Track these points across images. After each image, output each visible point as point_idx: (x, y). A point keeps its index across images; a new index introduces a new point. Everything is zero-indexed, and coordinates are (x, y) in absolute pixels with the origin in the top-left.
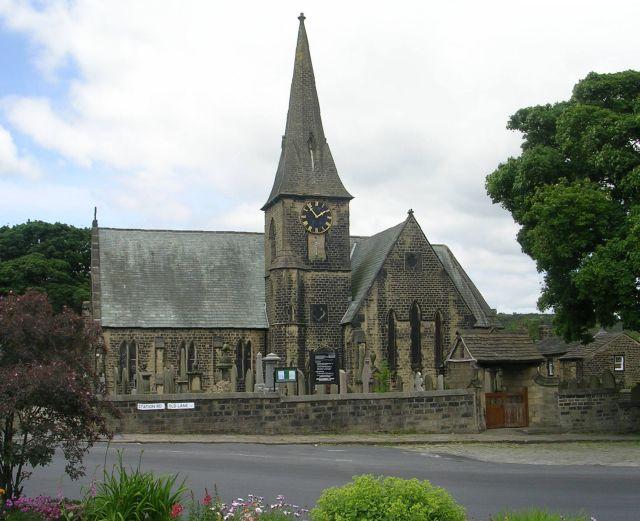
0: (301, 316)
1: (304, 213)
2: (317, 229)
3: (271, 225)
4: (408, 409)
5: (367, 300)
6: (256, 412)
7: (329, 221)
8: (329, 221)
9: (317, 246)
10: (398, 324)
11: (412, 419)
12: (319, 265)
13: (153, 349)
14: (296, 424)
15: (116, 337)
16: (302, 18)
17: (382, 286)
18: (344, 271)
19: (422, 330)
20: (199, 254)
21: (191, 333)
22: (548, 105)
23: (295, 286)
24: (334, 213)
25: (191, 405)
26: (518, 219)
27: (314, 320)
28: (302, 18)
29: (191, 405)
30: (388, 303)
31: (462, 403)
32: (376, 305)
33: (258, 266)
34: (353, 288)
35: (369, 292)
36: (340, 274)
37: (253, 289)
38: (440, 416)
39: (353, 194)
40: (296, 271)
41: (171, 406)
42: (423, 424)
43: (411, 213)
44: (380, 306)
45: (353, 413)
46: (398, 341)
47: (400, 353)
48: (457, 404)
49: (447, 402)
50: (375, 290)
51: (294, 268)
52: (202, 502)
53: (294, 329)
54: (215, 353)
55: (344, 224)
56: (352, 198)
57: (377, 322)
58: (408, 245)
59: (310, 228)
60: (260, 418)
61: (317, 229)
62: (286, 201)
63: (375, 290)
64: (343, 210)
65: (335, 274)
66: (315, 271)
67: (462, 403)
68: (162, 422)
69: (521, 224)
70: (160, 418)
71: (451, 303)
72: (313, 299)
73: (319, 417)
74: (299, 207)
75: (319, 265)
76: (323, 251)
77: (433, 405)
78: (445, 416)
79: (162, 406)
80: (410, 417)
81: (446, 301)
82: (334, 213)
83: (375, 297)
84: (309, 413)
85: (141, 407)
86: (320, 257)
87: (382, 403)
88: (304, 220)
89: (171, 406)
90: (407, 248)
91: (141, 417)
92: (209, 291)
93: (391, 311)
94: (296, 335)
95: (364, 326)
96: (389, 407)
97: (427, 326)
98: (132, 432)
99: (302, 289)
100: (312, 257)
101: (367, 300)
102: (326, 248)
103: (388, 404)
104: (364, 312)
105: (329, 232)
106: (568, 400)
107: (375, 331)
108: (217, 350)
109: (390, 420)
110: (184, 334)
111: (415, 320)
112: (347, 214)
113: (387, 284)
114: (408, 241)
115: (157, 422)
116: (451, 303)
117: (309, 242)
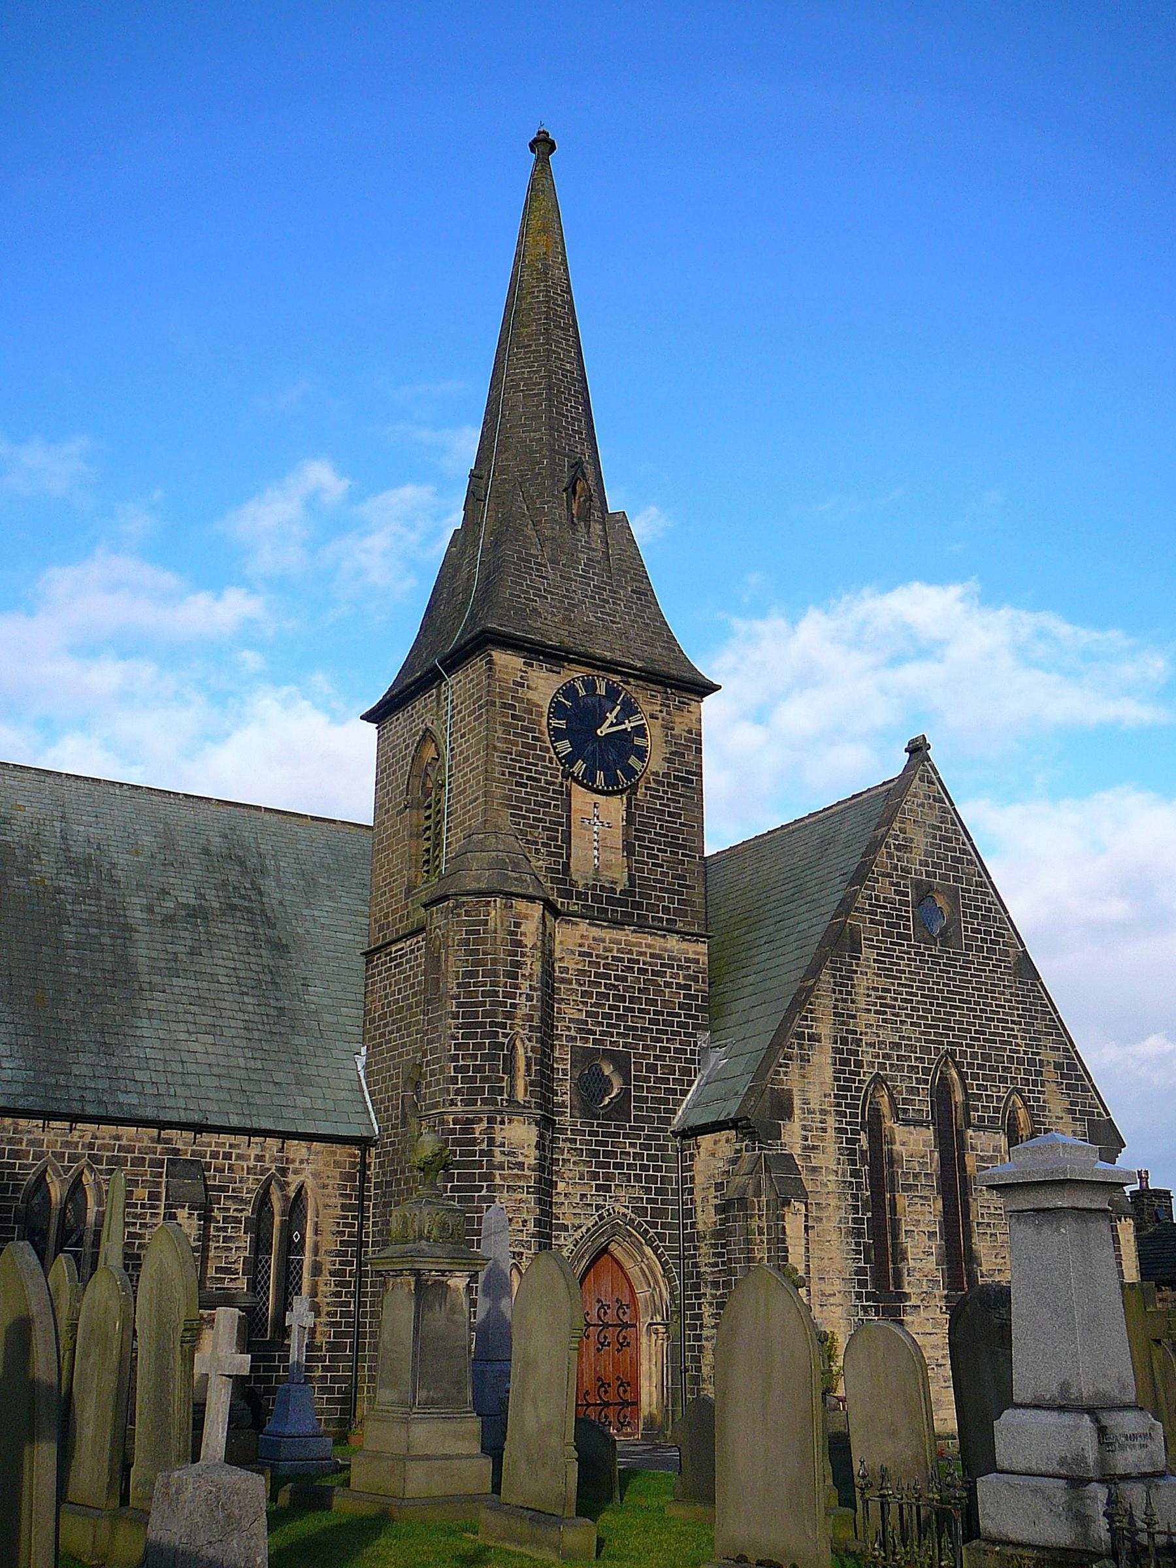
0: (544, 1083)
2: (600, 775)
3: (411, 782)
5: (788, 1038)
10: (900, 1132)
16: (543, 145)
17: (844, 985)
20: (122, 859)
23: (532, 966)
26: (260, 1472)
28: (543, 145)
33: (331, 931)
37: (316, 994)
39: (707, 669)
40: (537, 909)
43: (918, 749)
46: (902, 1200)
47: (907, 1242)
50: (824, 1004)
51: (531, 899)
52: (878, 1476)
53: (521, 1134)
55: (686, 780)
56: (713, 688)
57: (831, 1122)
58: (918, 855)
59: (579, 767)
61: (600, 775)
62: (501, 657)
66: (593, 920)
71: (1049, 1073)
74: (544, 686)
76: (617, 858)
82: (655, 731)
83: (825, 1029)
86: (607, 875)
88: (557, 734)
92: (152, 988)
93: (878, 1080)
95: (792, 1136)
102: (628, 848)
104: (792, 1080)
107: (829, 1157)
112: (695, 741)
116: (1049, 1073)
117: (575, 817)
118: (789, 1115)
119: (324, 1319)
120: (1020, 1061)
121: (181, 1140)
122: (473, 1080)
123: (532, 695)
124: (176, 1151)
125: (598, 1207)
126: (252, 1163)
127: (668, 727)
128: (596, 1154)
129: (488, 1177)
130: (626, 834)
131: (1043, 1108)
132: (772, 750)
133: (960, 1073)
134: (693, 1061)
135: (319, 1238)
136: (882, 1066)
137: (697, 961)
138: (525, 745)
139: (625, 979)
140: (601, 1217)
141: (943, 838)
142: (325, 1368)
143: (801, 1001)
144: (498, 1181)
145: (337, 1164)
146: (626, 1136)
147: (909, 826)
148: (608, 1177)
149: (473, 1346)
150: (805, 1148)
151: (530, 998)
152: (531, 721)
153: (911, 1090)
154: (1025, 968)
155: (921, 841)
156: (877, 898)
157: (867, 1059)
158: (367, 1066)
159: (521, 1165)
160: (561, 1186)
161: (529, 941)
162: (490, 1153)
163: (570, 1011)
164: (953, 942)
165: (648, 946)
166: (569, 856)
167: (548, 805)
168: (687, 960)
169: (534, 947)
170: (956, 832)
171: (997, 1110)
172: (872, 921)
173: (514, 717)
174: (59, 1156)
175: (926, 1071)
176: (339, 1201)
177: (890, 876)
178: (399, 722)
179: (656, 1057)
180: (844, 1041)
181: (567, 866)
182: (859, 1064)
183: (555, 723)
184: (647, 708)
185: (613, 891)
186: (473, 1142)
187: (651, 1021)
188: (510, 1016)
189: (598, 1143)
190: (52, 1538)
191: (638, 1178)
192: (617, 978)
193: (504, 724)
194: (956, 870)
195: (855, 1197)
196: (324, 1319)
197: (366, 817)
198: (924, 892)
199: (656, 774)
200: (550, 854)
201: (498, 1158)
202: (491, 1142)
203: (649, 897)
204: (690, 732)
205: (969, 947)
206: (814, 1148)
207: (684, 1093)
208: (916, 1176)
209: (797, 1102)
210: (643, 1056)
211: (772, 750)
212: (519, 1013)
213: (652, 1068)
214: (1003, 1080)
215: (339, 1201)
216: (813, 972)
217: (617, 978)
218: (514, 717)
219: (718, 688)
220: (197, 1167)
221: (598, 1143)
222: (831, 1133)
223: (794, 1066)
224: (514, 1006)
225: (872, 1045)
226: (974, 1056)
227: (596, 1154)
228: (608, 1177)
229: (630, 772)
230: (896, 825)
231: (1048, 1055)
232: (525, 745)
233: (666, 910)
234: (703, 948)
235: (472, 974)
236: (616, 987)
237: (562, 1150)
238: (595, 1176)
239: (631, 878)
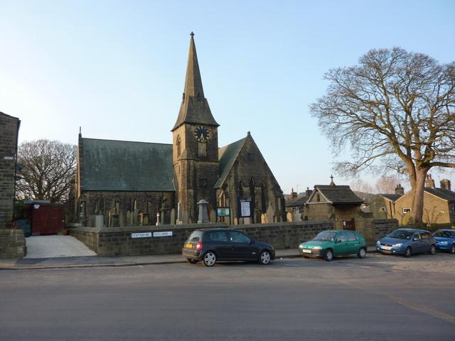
4: (301, 232)
9: (202, 149)
12: (203, 159)
16: (192, 34)
19: (255, 191)
21: (135, 193)
24: (210, 133)
25: (170, 233)
28: (192, 34)
29: (170, 233)
30: (239, 178)
34: (220, 171)
35: (230, 172)
36: (214, 163)
39: (219, 123)
43: (249, 133)
44: (235, 179)
45: (270, 236)
54: (148, 204)
63: (233, 172)
68: (150, 247)
69: (232, 147)
70: (148, 244)
75: (203, 159)
76: (205, 152)
77: (313, 230)
79: (150, 235)
81: (266, 177)
83: (233, 175)
85: (134, 236)
90: (248, 150)
94: (192, 194)
95: (228, 189)
96: (290, 231)
97: (258, 189)
98: (128, 255)
99: (195, 171)
101: (229, 176)
103: (290, 229)
104: (228, 182)
106: (378, 226)
107: (233, 192)
109: (290, 240)
110: (131, 194)
112: (216, 134)
114: (248, 147)
115: (146, 247)
121: (149, 193)
149: (158, 215)
163: (199, 174)
178: (175, 132)
190: (154, 265)
198: (249, 154)
220: (151, 196)
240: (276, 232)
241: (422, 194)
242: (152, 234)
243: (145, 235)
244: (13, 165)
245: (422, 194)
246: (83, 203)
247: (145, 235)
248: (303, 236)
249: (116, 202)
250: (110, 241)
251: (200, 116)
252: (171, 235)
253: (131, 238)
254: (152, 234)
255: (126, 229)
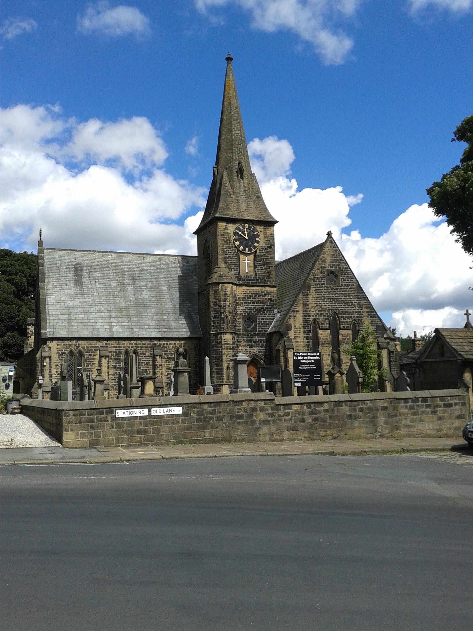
1: (236, 234)
2: (247, 249)
4: (405, 411)
6: (250, 416)
7: (258, 242)
8: (258, 242)
10: (320, 332)
11: (408, 422)
12: (249, 282)
13: (97, 357)
14: (292, 429)
15: (62, 346)
17: (306, 298)
18: (270, 287)
19: (341, 338)
22: (464, 141)
25: (178, 410)
27: (246, 330)
29: (178, 410)
30: (312, 314)
31: (456, 404)
32: (301, 315)
36: (267, 289)
38: (435, 419)
41: (156, 412)
42: (420, 427)
43: (329, 234)
45: (350, 417)
48: (450, 405)
49: (442, 403)
56: (276, 222)
57: (302, 330)
58: (328, 262)
59: (241, 248)
60: (253, 422)
61: (247, 249)
64: (269, 232)
65: (263, 289)
66: (246, 286)
67: (456, 404)
70: (142, 427)
71: (365, 314)
72: (245, 311)
73: (315, 420)
78: (440, 418)
79: (145, 412)
80: (406, 419)
81: (361, 313)
82: (262, 235)
83: (300, 308)
84: (306, 417)
85: (120, 414)
87: (380, 404)
88: (236, 240)
89: (156, 412)
91: (119, 426)
93: (315, 320)
94: (231, 342)
96: (384, 408)
97: (345, 334)
100: (242, 275)
102: (255, 266)
103: (385, 405)
104: (292, 322)
105: (258, 252)
107: (301, 338)
108: (158, 358)
111: (335, 328)
112: (272, 237)
113: (310, 297)
115: (139, 432)
116: (365, 314)
118: (291, 329)
119: (193, 379)
120: (356, 312)
122: (217, 326)
123: (229, 231)
124: (155, 344)
125: (250, 352)
126: (173, 345)
127: (265, 234)
128: (249, 340)
129: (221, 347)
130: (254, 263)
131: (363, 323)
132: (288, 241)
133: (338, 316)
134: (273, 316)
135: (99, 368)
136: (316, 316)
137: (274, 292)
138: (227, 244)
139: (255, 298)
140: (250, 354)
141: (335, 257)
142: (193, 389)
143: (294, 302)
144: (223, 348)
145: (193, 344)
146: (256, 335)
147: (325, 256)
148: (252, 345)
150: (295, 337)
151: (229, 306)
152: (229, 238)
153: (324, 321)
154: (359, 288)
155: (329, 259)
156: (315, 275)
157: (312, 315)
158: (200, 320)
159: (229, 344)
160: (240, 348)
161: (228, 293)
162: (221, 342)
164: (337, 284)
165: (261, 290)
166: (239, 270)
167: (234, 258)
168: (271, 292)
169: (230, 294)
170: (339, 255)
171: (348, 324)
172: (314, 281)
173: (224, 238)
174: (129, 347)
175: (328, 316)
176: (194, 352)
177: (319, 269)
179: (263, 316)
180: (306, 311)
181: (239, 273)
182: (310, 316)
183: (235, 237)
184: (259, 230)
185: (251, 277)
186: (218, 339)
187: (262, 308)
188: (225, 311)
189: (249, 337)
191: (259, 345)
192: (253, 298)
193: (221, 240)
194: (339, 265)
195: (308, 347)
196: (193, 379)
197: (196, 254)
199: (262, 247)
200: (235, 270)
201: (223, 343)
202: (221, 339)
203: (261, 278)
204: (271, 234)
205: (342, 285)
206: (297, 337)
207: (271, 324)
208: (325, 341)
209: (293, 327)
210: (260, 316)
211: (288, 241)
212: (227, 310)
213: (262, 319)
214: (351, 317)
215: (194, 352)
216: (298, 294)
217: (253, 298)
218: (224, 238)
219: (278, 222)
221: (249, 337)
222: (302, 333)
223: (292, 318)
224: (225, 308)
225: (313, 311)
226: (342, 312)
227: (249, 340)
228: (252, 345)
229: (255, 247)
230: (322, 256)
231: (365, 310)
232: (227, 244)
233: (265, 281)
234: (275, 289)
235: (216, 302)
236: (253, 301)
237: (240, 340)
238: (248, 345)
239: (256, 274)
240: (361, 410)
241: (154, 373)
242: (150, 411)
243: (137, 413)
244: (249, 230)
245: (154, 373)
246: (48, 360)
247: (137, 413)
248: (410, 417)
249: (101, 357)
250: (80, 422)
251: (244, 206)
252: (181, 412)
253: (114, 419)
254: (150, 411)
255: (108, 403)
